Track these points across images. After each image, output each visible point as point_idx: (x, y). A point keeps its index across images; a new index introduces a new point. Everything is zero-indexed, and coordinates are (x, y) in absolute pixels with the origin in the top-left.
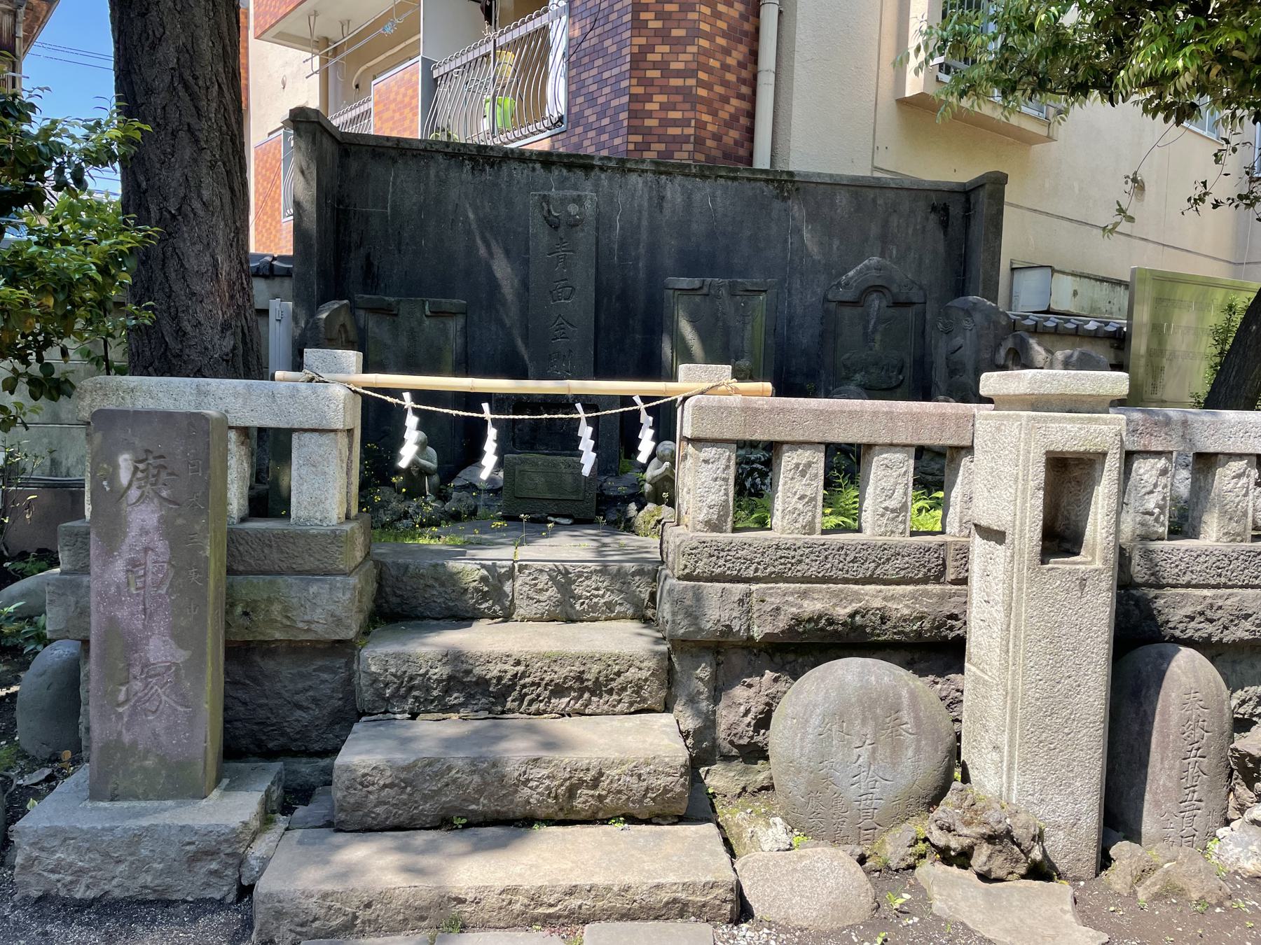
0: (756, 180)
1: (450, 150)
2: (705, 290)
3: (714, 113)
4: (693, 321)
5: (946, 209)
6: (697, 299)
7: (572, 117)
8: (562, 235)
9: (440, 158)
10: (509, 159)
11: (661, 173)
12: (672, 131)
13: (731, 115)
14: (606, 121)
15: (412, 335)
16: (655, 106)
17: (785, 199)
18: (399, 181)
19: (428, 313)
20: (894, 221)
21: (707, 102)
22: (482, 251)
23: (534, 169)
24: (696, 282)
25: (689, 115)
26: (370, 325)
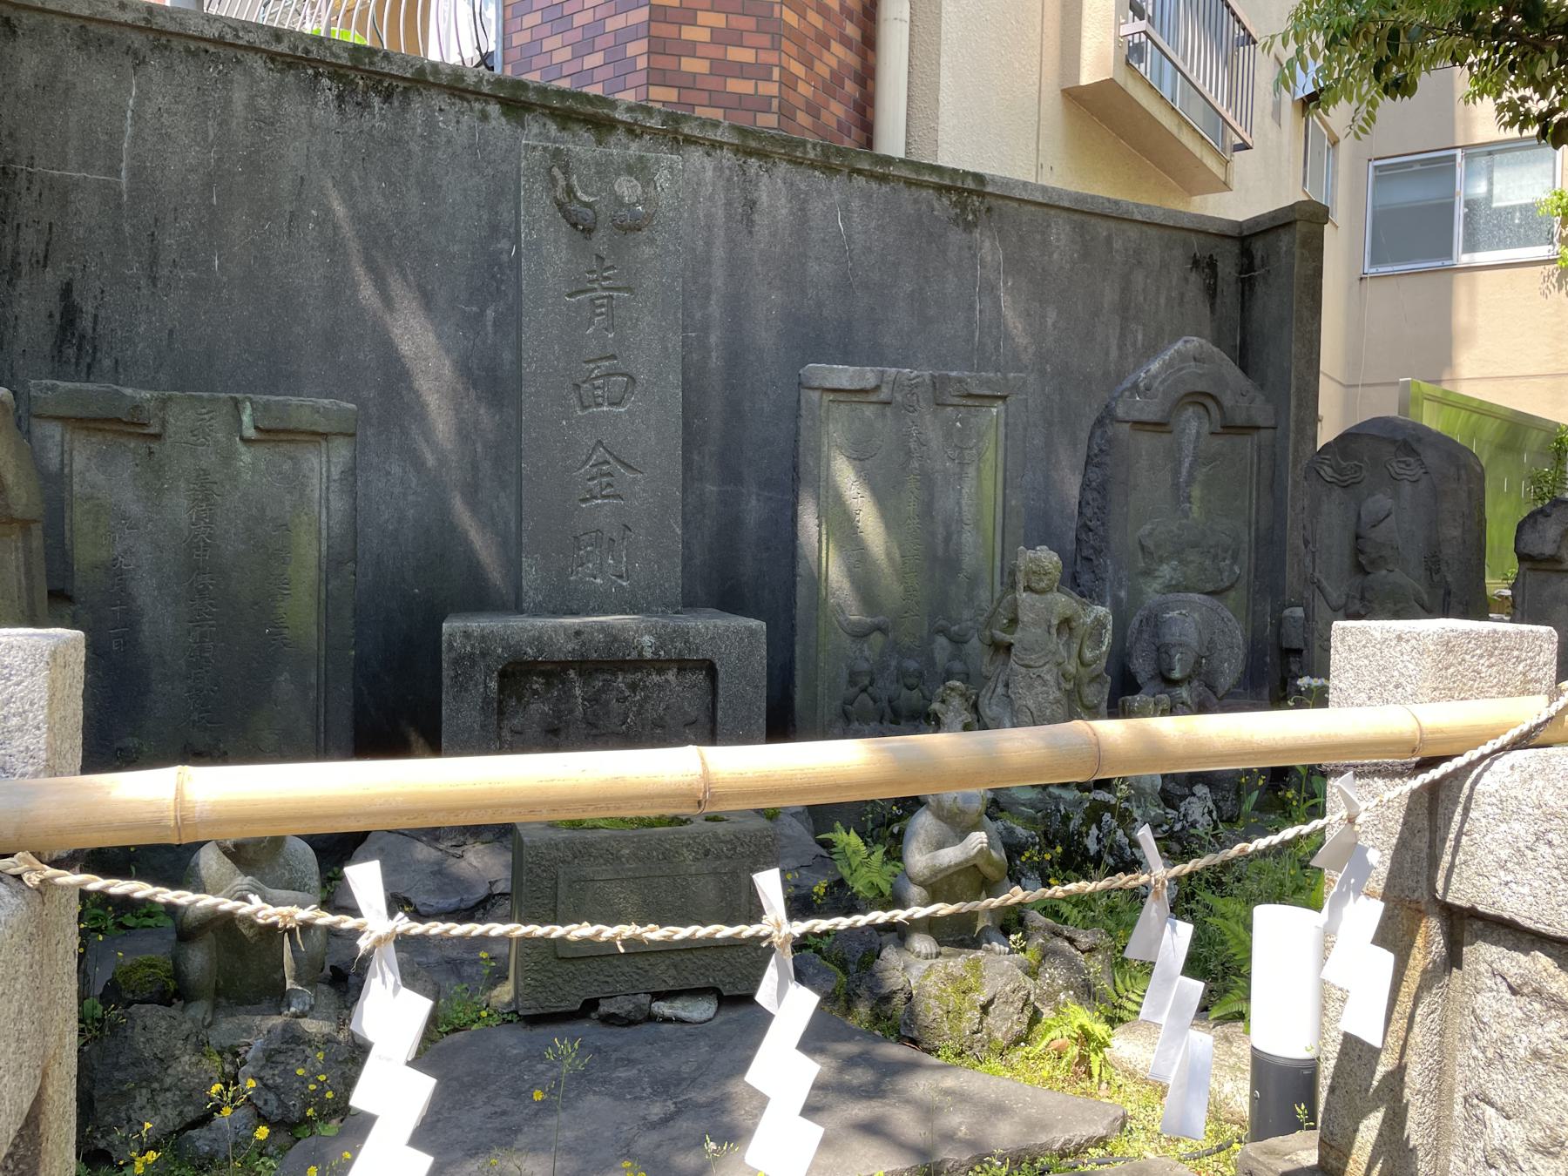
0: (920, 185)
1: (283, 48)
2: (884, 394)
3: (808, 64)
4: (860, 457)
5: (1212, 264)
6: (869, 411)
7: (514, 54)
8: (603, 249)
9: (258, 64)
10: (430, 85)
11: (750, 153)
12: (736, 86)
13: (833, 72)
14: (595, 60)
15: (204, 489)
16: (702, 35)
17: (969, 227)
18: (150, 109)
19: (250, 432)
20: (1139, 278)
21: (798, 38)
22: (367, 292)
23: (484, 117)
24: (869, 376)
25: (769, 57)
26: (79, 462)
